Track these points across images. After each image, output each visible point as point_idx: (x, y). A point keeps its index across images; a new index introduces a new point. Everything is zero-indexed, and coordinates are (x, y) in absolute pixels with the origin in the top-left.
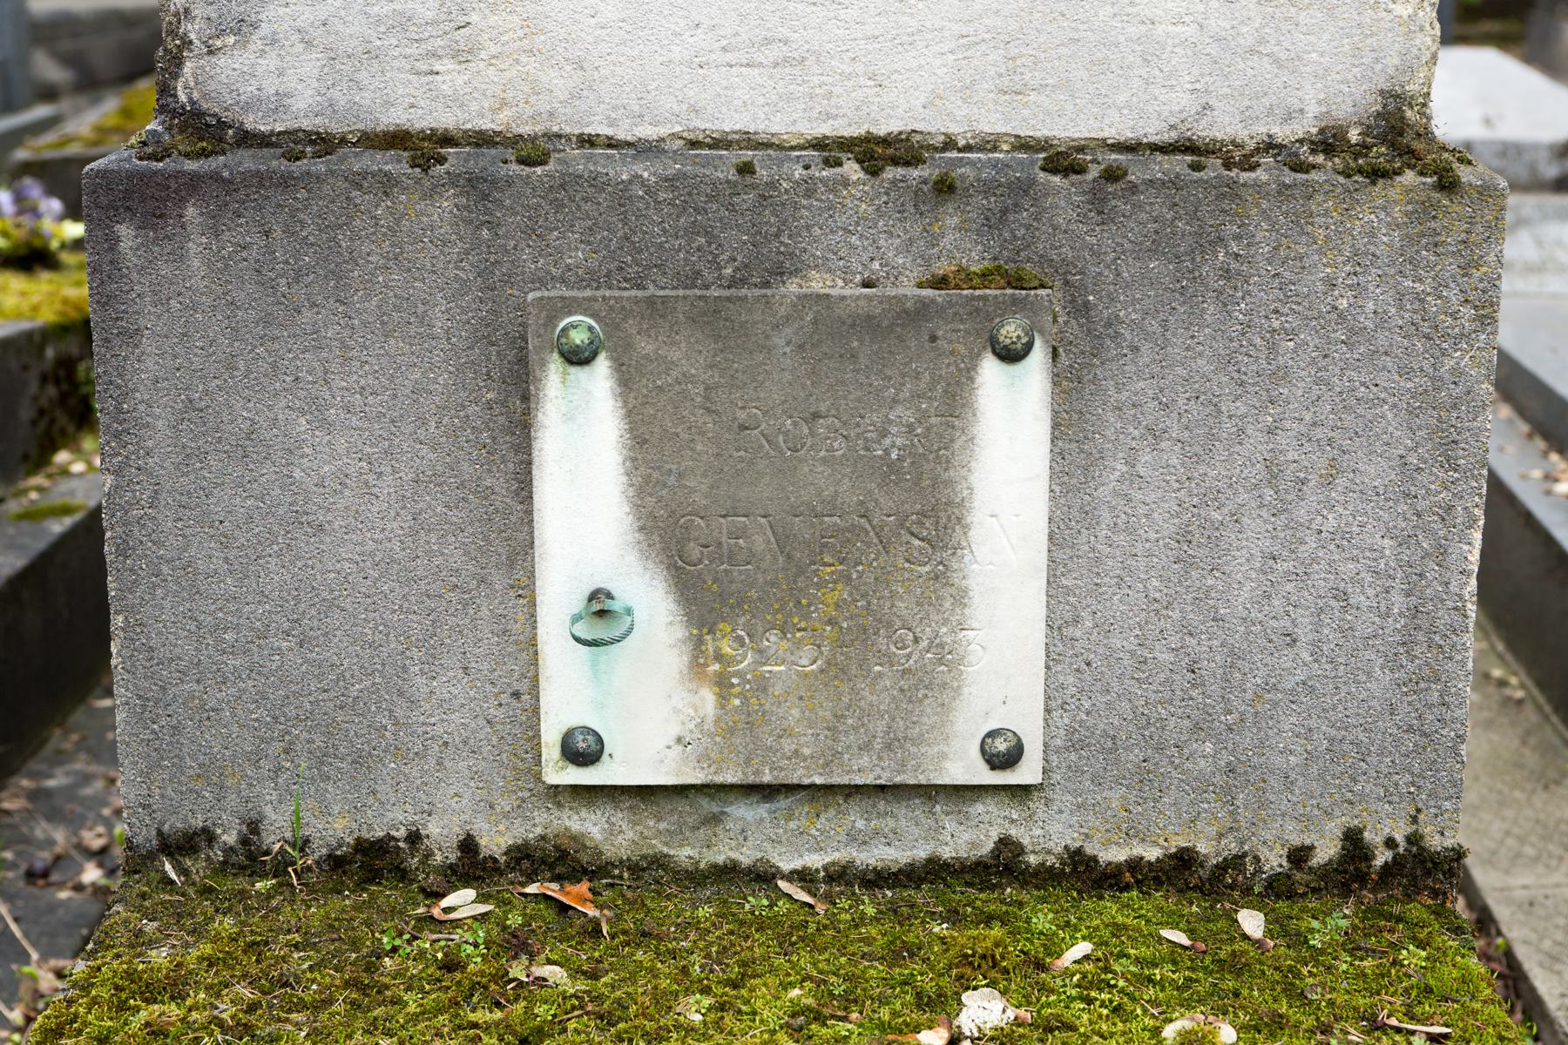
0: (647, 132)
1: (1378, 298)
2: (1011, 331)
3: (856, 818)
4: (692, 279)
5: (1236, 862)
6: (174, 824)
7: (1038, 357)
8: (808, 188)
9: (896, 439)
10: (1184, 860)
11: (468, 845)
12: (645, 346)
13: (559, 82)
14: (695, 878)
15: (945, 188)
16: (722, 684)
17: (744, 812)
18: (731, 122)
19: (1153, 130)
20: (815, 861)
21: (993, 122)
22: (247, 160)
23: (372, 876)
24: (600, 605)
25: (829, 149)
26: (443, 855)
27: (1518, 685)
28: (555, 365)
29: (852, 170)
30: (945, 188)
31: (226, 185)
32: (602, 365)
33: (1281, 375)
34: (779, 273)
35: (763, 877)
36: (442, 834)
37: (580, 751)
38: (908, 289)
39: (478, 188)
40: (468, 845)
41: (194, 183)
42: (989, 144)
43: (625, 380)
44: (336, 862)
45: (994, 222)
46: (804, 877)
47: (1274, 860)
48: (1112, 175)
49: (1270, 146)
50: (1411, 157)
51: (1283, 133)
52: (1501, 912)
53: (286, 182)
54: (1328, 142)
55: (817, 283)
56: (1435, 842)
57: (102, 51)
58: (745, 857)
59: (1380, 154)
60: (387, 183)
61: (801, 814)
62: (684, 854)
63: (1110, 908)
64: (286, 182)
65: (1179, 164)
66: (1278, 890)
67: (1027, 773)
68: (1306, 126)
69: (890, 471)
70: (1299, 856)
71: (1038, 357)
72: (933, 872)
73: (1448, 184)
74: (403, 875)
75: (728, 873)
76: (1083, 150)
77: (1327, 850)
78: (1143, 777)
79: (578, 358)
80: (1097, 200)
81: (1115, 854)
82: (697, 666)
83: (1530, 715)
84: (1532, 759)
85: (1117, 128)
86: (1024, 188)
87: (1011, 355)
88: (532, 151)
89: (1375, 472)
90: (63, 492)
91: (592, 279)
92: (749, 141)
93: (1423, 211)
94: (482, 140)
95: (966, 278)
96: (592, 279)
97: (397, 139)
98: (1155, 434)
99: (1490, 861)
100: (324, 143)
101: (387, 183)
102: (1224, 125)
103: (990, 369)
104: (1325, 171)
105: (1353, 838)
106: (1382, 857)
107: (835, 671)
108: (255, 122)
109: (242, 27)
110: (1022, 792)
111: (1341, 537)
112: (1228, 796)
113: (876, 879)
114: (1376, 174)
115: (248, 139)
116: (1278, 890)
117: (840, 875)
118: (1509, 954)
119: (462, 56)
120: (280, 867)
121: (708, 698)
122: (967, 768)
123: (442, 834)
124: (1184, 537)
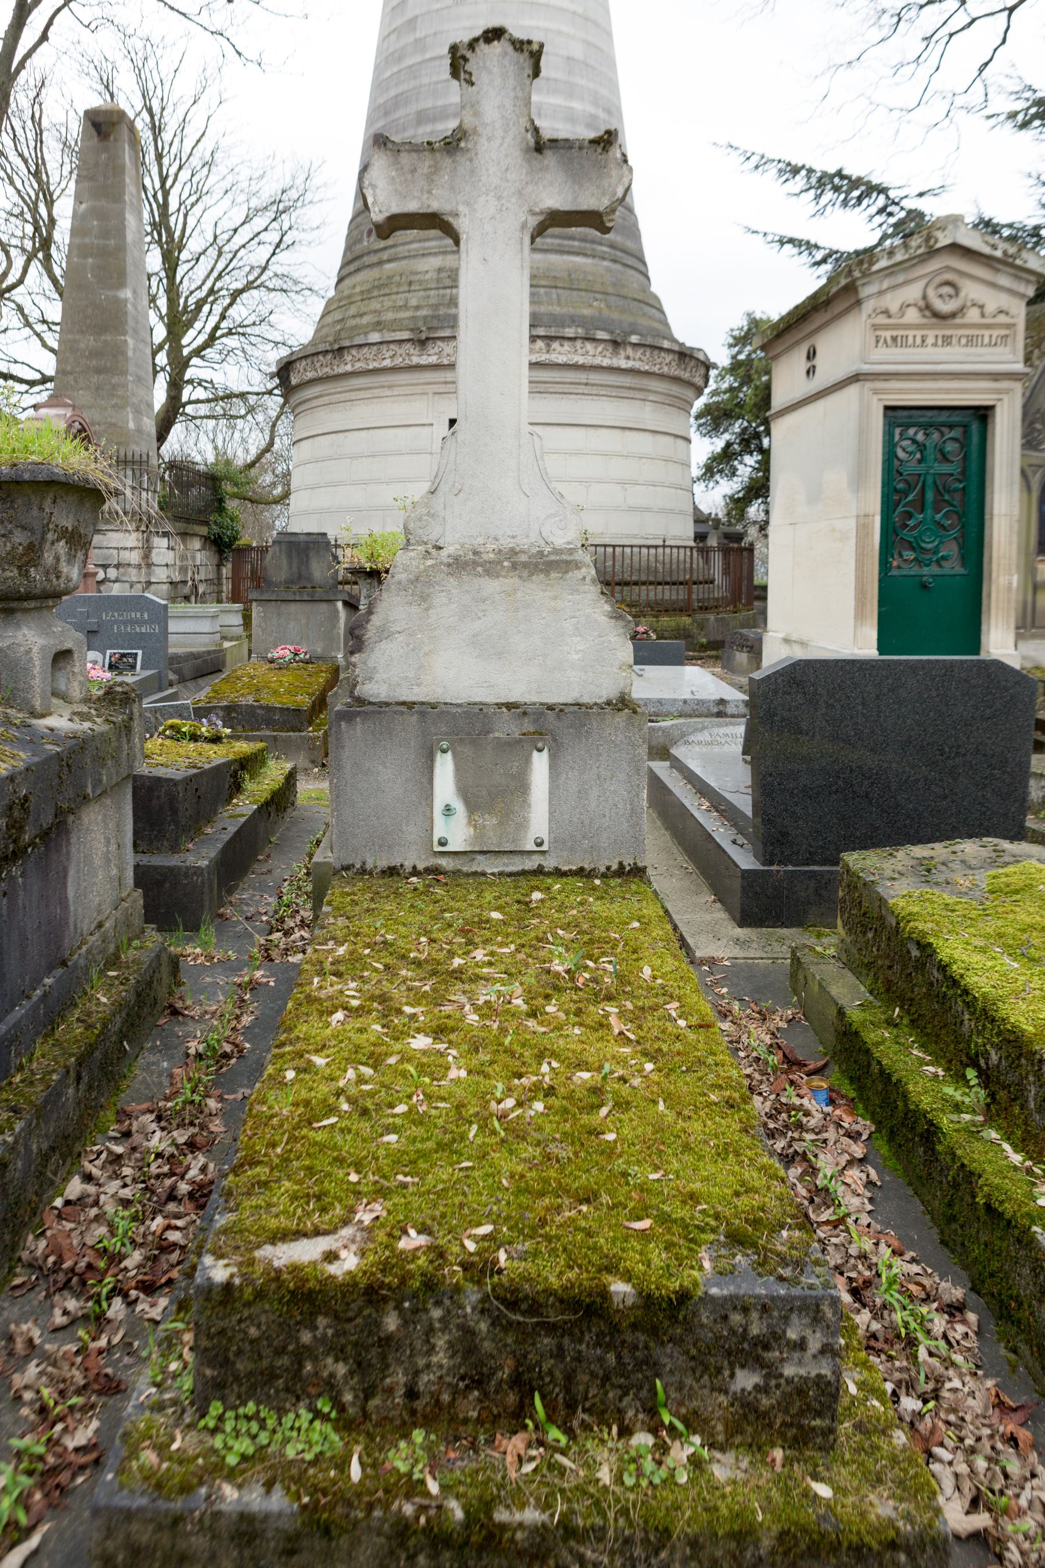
0: (459, 701)
1: (621, 737)
2: (540, 745)
3: (505, 859)
4: (469, 734)
5: (594, 870)
6: (345, 863)
7: (546, 750)
8: (495, 714)
9: (515, 769)
10: (582, 869)
11: (414, 867)
12: (459, 749)
13: (440, 691)
14: (468, 875)
15: (525, 713)
16: (475, 826)
17: (480, 857)
18: (477, 699)
19: (570, 701)
20: (496, 870)
21: (535, 699)
22: (370, 708)
23: (391, 875)
24: (448, 810)
25: (499, 705)
26: (409, 869)
27: (691, 868)
28: (439, 753)
29: (504, 710)
30: (525, 713)
31: (366, 713)
32: (450, 753)
33: (600, 755)
34: (489, 732)
35: (484, 874)
36: (408, 865)
37: (443, 843)
38: (517, 735)
39: (422, 714)
40: (414, 867)
41: (359, 713)
42: (534, 704)
43: (454, 756)
44: (383, 872)
45: (535, 721)
46: (493, 874)
47: (603, 869)
48: (561, 711)
49: (596, 704)
50: (627, 706)
51: (599, 701)
52: (679, 924)
53: (380, 713)
54: (609, 703)
55: (497, 735)
56: (640, 865)
57: (187, 668)
58: (479, 870)
59: (620, 706)
60: (402, 713)
61: (492, 859)
62: (465, 869)
63: (564, 880)
64: (380, 713)
65: (576, 708)
66: (604, 876)
67: (545, 848)
68: (603, 700)
69: (513, 777)
70: (608, 868)
71: (546, 750)
72: (523, 873)
73: (635, 712)
74: (399, 874)
75: (475, 874)
76: (324, 1046)
77: (615, 867)
78: (572, 849)
79: (444, 751)
80: (558, 716)
81: (565, 868)
82: (469, 823)
83: (694, 876)
84: (693, 888)
85: (562, 700)
86: (542, 713)
87: (540, 750)
88: (433, 706)
89: (622, 776)
90: (238, 811)
91: (447, 734)
92: (481, 703)
93: (630, 718)
94: (422, 703)
95: (530, 733)
96: (447, 734)
97: (404, 703)
98: (572, 768)
99: (678, 913)
100: (387, 704)
101: (402, 713)
102: (586, 699)
103: (535, 753)
104: (608, 709)
105: (621, 864)
106: (628, 868)
107: (501, 823)
108: (372, 700)
109: (370, 679)
110: (543, 852)
111: (615, 792)
112: (591, 853)
113: (510, 875)
114: (619, 710)
115: (370, 703)
116: (604, 876)
117: (501, 874)
118: (681, 935)
119: (418, 685)
120: (371, 873)
121: (472, 830)
122: (531, 846)
123: (408, 865)
124: (579, 792)
